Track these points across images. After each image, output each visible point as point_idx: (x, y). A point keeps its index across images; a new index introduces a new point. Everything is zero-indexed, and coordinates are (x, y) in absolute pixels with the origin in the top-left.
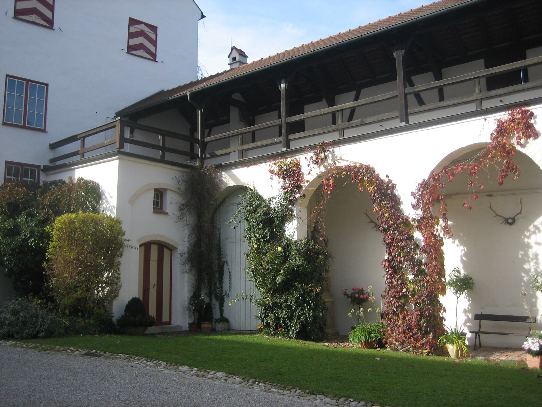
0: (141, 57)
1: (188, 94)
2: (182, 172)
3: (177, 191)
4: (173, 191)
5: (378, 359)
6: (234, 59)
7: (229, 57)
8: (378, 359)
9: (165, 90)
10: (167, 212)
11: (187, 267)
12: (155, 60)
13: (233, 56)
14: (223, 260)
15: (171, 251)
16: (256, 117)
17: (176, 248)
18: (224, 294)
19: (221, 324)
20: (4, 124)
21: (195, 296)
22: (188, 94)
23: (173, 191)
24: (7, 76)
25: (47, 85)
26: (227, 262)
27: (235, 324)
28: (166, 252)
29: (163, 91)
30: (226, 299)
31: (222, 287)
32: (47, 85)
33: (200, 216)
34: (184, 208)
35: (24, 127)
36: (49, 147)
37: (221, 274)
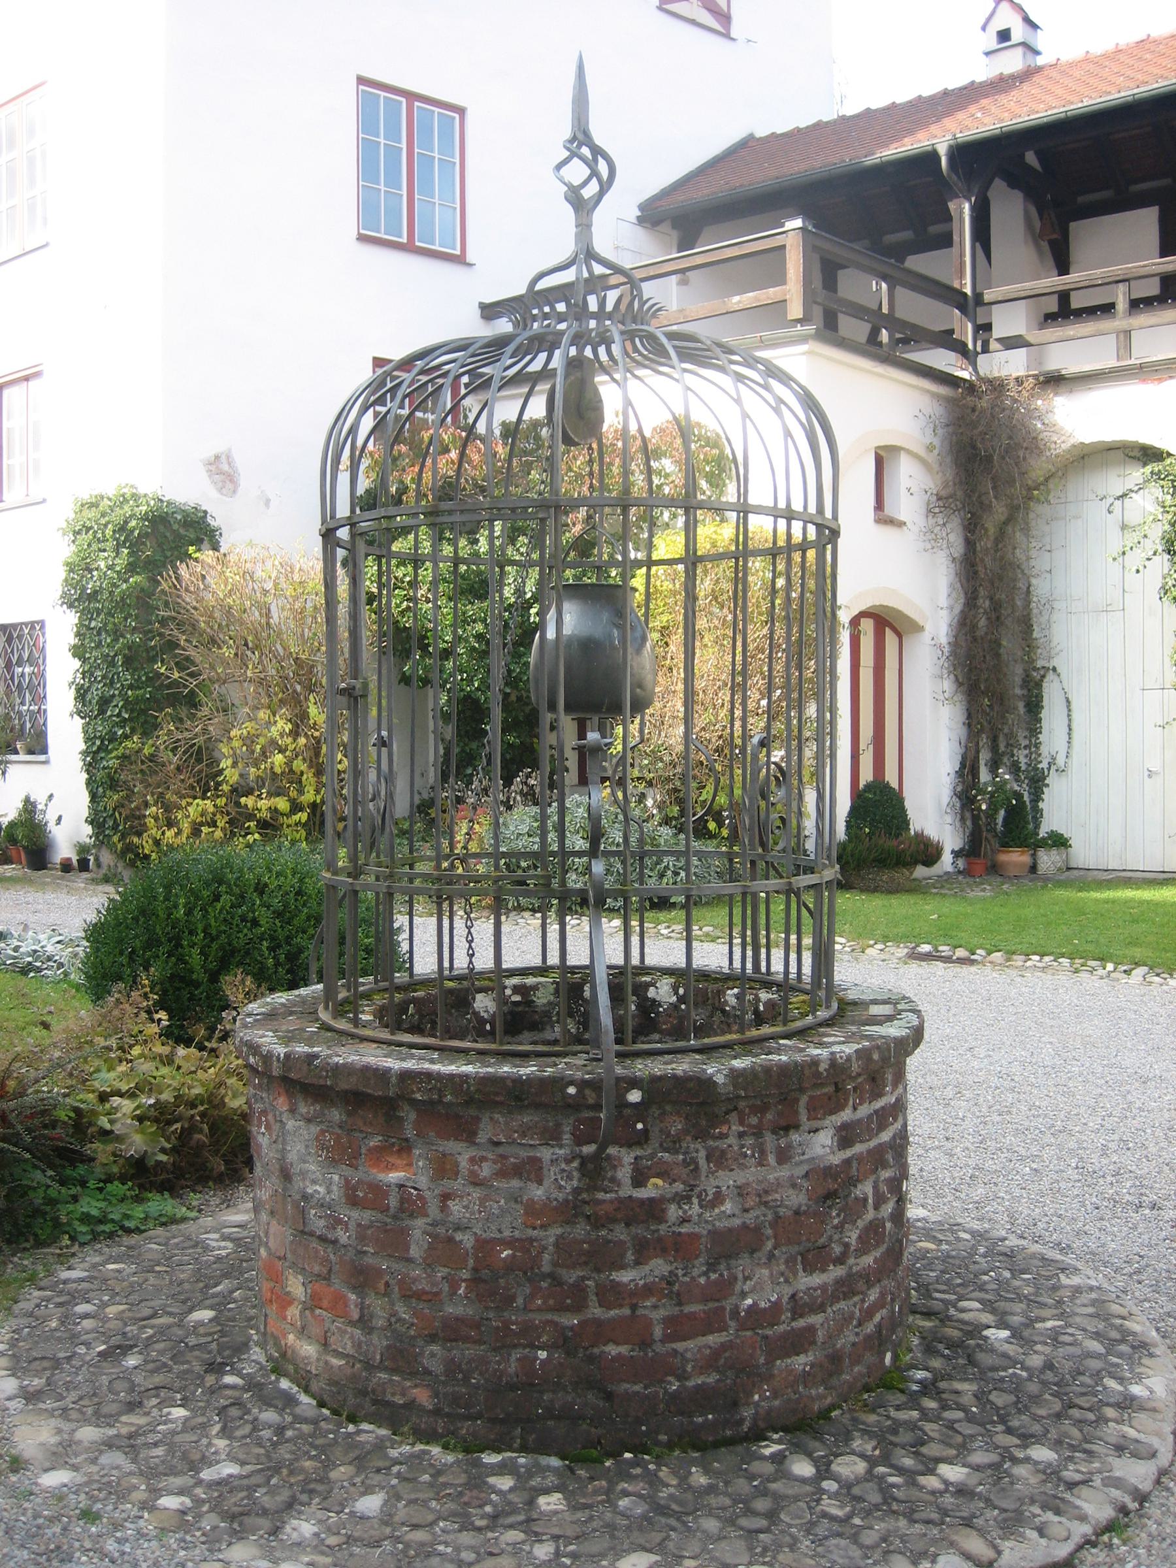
0: (693, 22)
1: (942, 150)
2: (934, 395)
3: (922, 452)
4: (916, 456)
5: (572, 1090)
6: (1004, 35)
7: (984, 28)
8: (572, 1090)
9: (761, 133)
10: (902, 518)
11: (948, 685)
12: (727, 36)
13: (999, 24)
14: (1039, 664)
15: (900, 636)
16: (1073, 225)
17: (917, 628)
18: (1044, 765)
19: (1054, 851)
20: (362, 238)
21: (967, 770)
22: (942, 150)
23: (916, 456)
24: (361, 80)
25: (461, 111)
26: (1054, 669)
27: (1083, 853)
28: (890, 638)
29: (751, 137)
30: (1052, 779)
31: (1037, 746)
32: (461, 111)
33: (972, 528)
34: (941, 504)
35: (408, 247)
36: (477, 312)
37: (1034, 706)
